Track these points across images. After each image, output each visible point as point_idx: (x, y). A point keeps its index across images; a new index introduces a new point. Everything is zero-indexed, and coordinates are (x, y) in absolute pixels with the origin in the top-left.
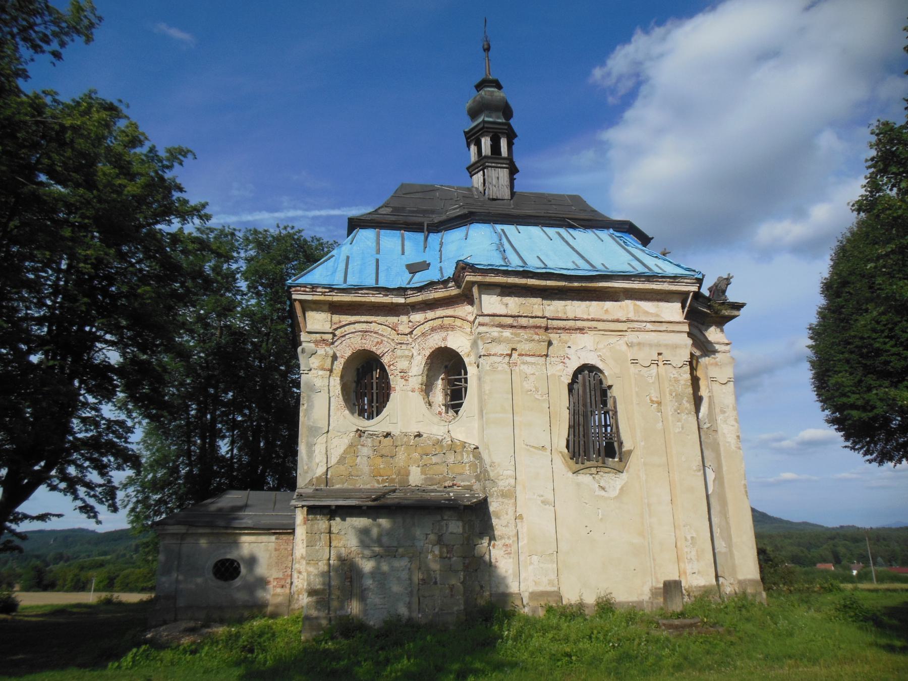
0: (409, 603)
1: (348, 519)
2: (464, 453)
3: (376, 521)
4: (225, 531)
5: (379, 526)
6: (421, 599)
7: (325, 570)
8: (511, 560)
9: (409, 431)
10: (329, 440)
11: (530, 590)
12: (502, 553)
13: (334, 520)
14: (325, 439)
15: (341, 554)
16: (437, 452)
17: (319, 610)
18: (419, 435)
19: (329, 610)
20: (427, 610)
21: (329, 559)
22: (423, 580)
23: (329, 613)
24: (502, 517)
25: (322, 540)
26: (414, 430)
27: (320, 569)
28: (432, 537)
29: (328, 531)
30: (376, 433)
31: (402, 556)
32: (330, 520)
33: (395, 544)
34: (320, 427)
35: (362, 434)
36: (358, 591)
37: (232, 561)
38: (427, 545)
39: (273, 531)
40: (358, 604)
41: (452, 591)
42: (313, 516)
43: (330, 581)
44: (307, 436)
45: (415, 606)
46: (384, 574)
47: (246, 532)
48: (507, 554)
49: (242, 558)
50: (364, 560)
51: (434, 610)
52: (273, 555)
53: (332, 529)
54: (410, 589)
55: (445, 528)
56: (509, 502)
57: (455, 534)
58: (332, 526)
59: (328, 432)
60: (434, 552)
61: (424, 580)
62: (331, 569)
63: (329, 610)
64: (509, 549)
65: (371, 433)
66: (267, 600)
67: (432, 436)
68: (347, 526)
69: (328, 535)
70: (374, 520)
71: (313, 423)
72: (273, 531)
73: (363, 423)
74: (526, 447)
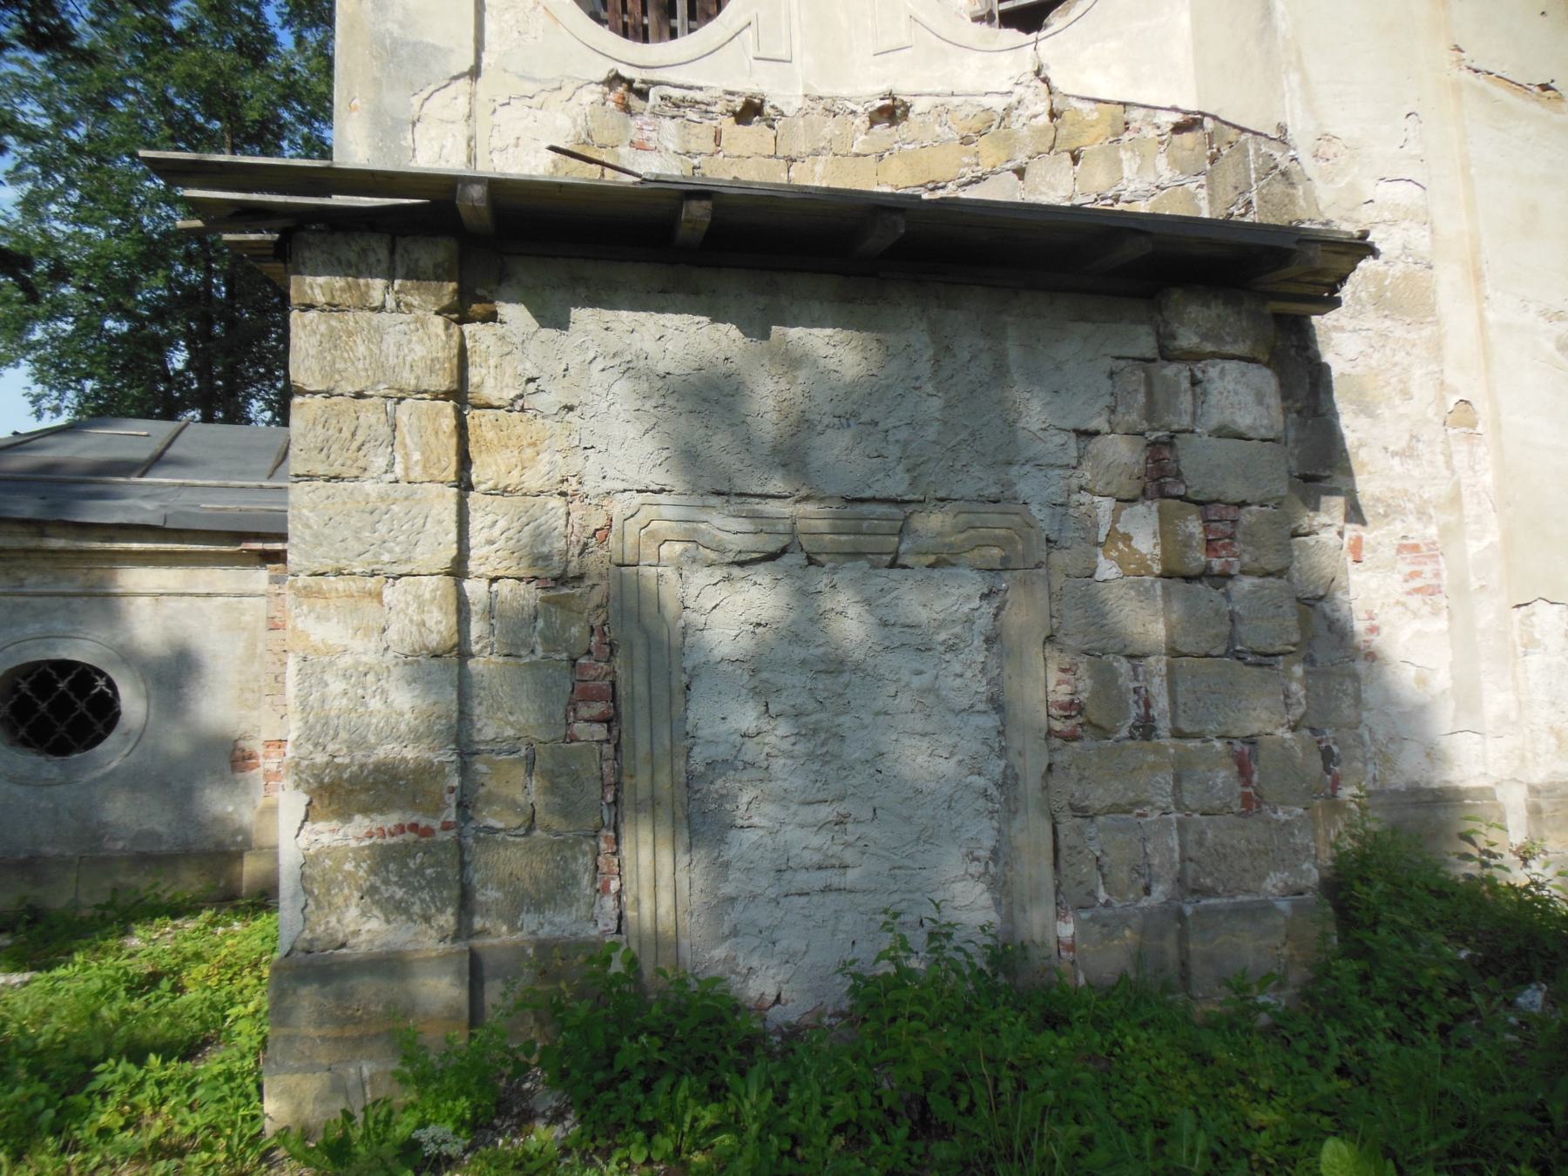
0: (995, 854)
1: (584, 318)
2: (1124, 155)
3: (765, 335)
4: (32, 543)
5: (792, 361)
6: (1067, 823)
7: (433, 640)
8: (1442, 624)
9: (845, 92)
10: (482, 112)
11: (1539, 777)
12: (1394, 584)
13: (491, 317)
14: (462, 105)
15: (540, 536)
16: (985, 168)
17: (395, 909)
18: (891, 112)
19: (465, 903)
20: (1103, 896)
21: (458, 569)
22: (1072, 708)
23: (463, 930)
24: (1383, 410)
25: (406, 434)
26: (868, 88)
27: (392, 635)
28: (1121, 452)
29: (443, 381)
30: (698, 96)
31: (942, 562)
32: (459, 313)
33: (896, 485)
34: (435, 48)
35: (635, 102)
36: (663, 779)
37: (84, 675)
38: (1085, 498)
39: (258, 546)
40: (665, 858)
41: (1244, 772)
42: (339, 282)
43: (464, 714)
44: (376, 82)
45: (1035, 868)
46: (835, 665)
47: (135, 546)
48: (1418, 590)
49: (129, 657)
50: (700, 578)
51: (1147, 891)
52: (260, 647)
53: (474, 376)
54: (997, 767)
55: (1186, 401)
56: (1413, 336)
57: (1240, 436)
58: (473, 359)
59: (475, 73)
60: (1127, 538)
61: (1081, 709)
62: (476, 628)
63: (465, 903)
64: (1428, 569)
65: (677, 94)
66: (241, 830)
67: (956, 101)
68: (575, 360)
69: (448, 407)
70: (757, 328)
71: (402, 26)
72: (258, 546)
73: (631, 56)
74: (1471, 76)
